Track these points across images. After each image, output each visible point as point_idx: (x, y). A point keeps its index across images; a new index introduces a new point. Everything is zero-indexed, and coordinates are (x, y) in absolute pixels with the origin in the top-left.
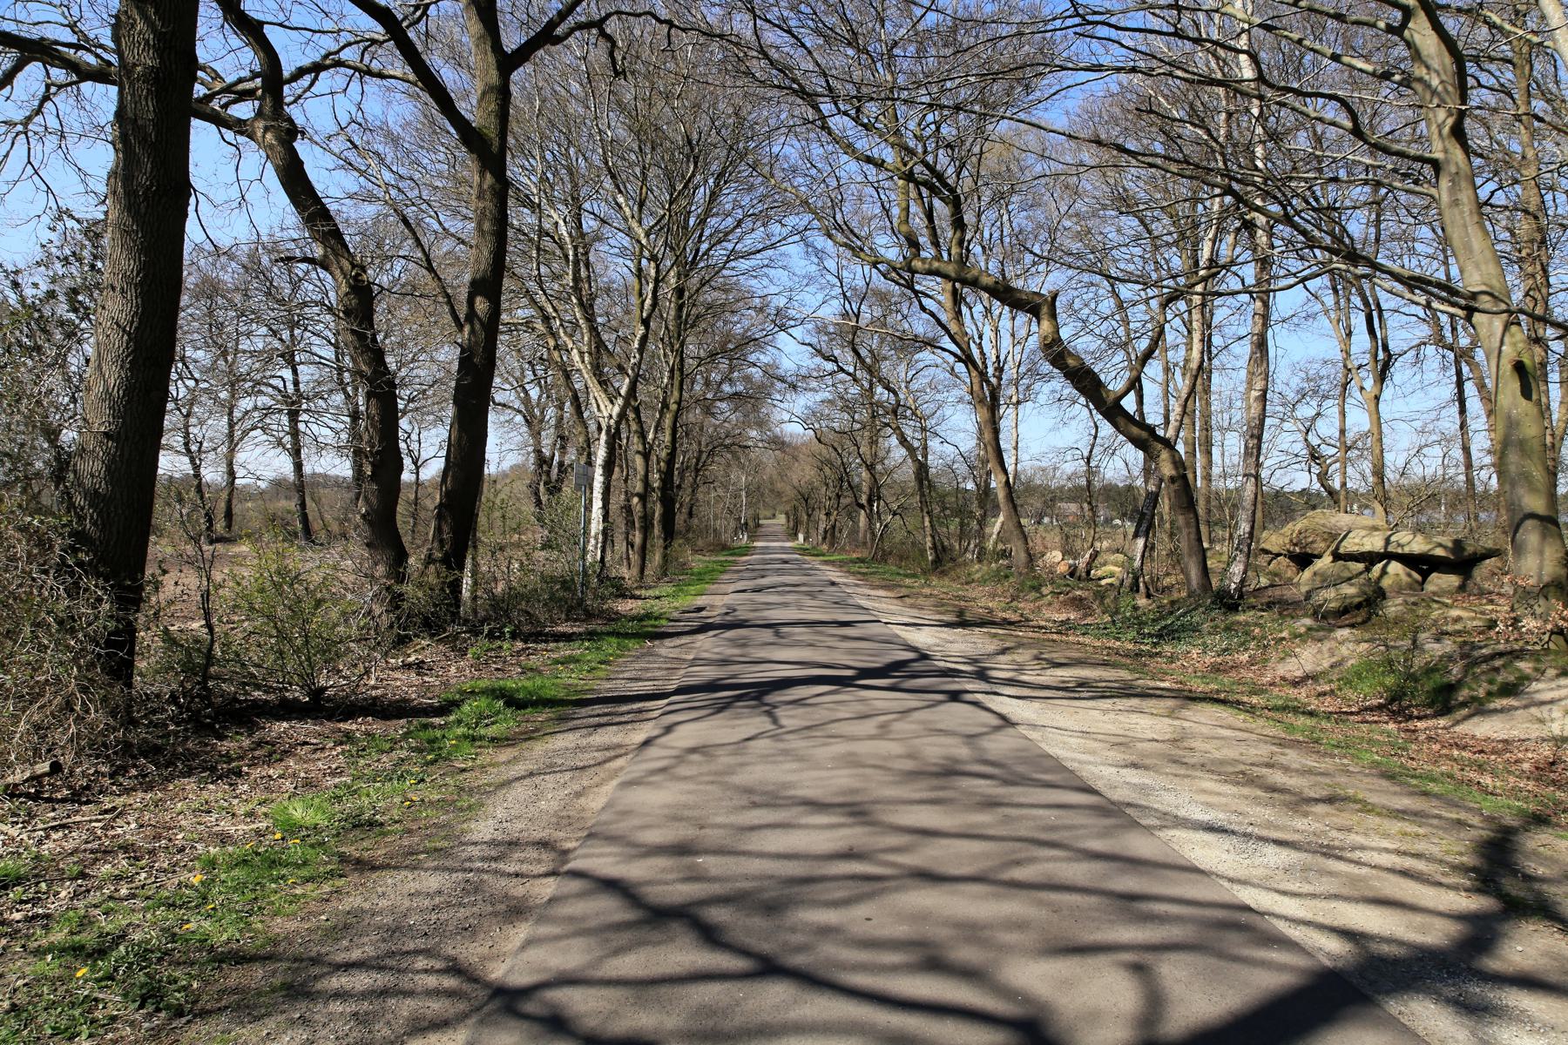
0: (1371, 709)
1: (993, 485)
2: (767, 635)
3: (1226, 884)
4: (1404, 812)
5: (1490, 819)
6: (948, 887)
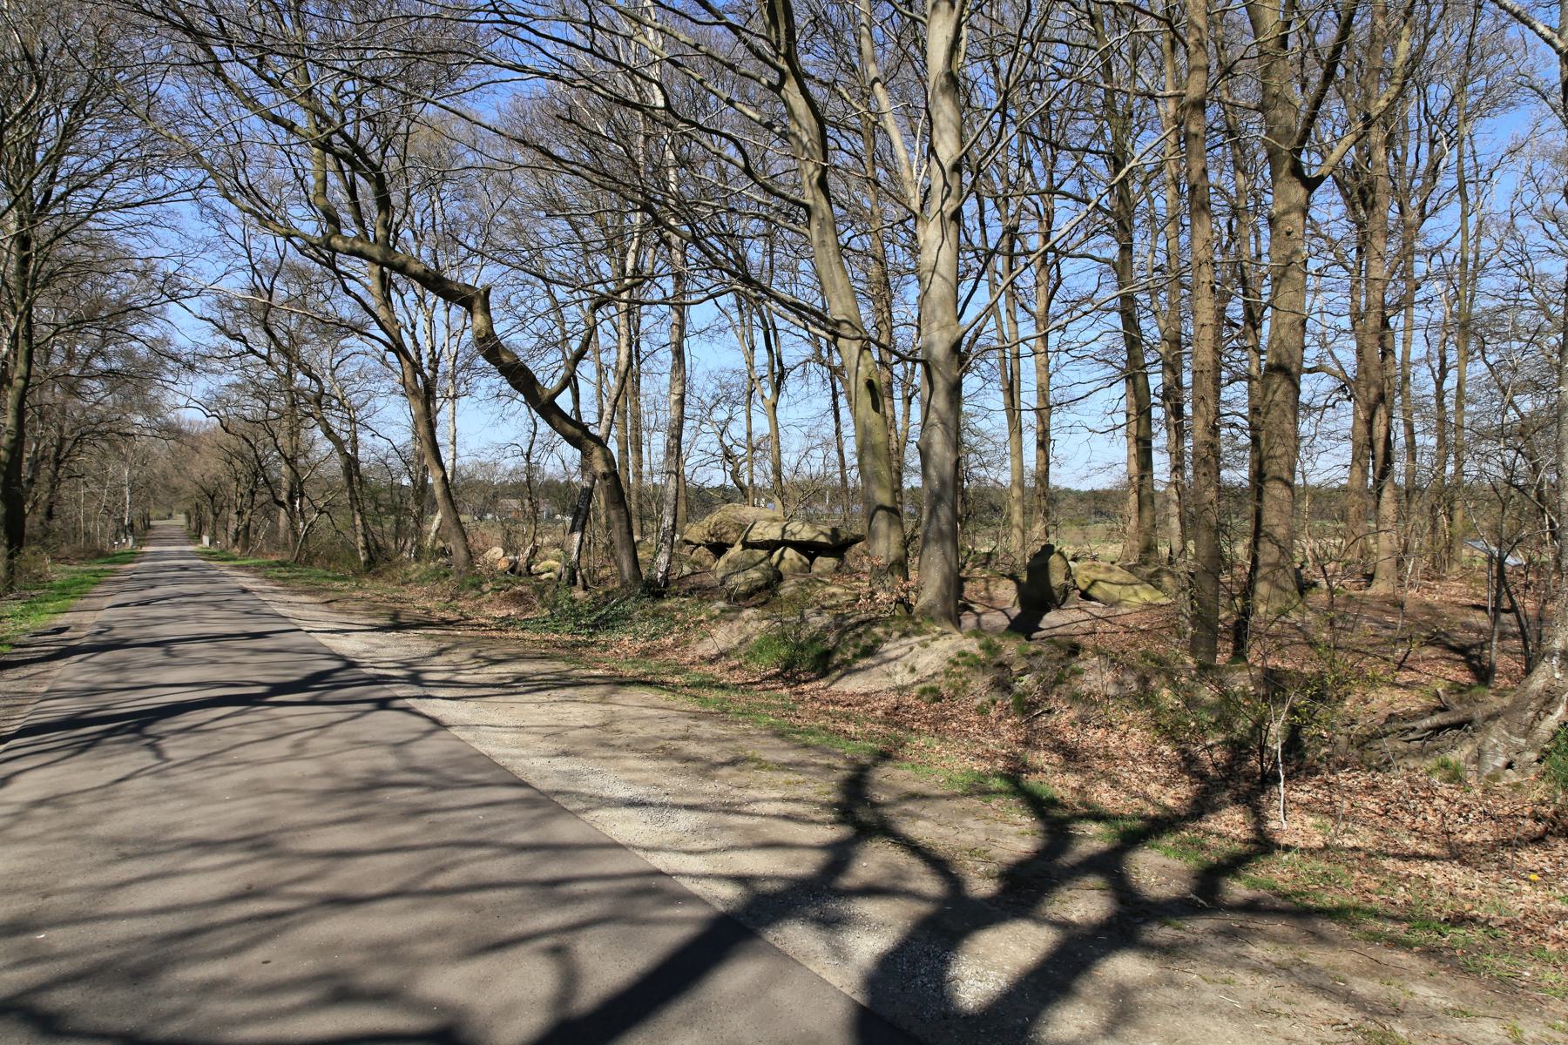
0: (769, 678)
1: (430, 481)
2: (156, 655)
3: (641, 854)
4: (789, 764)
5: (852, 760)
6: (363, 909)
